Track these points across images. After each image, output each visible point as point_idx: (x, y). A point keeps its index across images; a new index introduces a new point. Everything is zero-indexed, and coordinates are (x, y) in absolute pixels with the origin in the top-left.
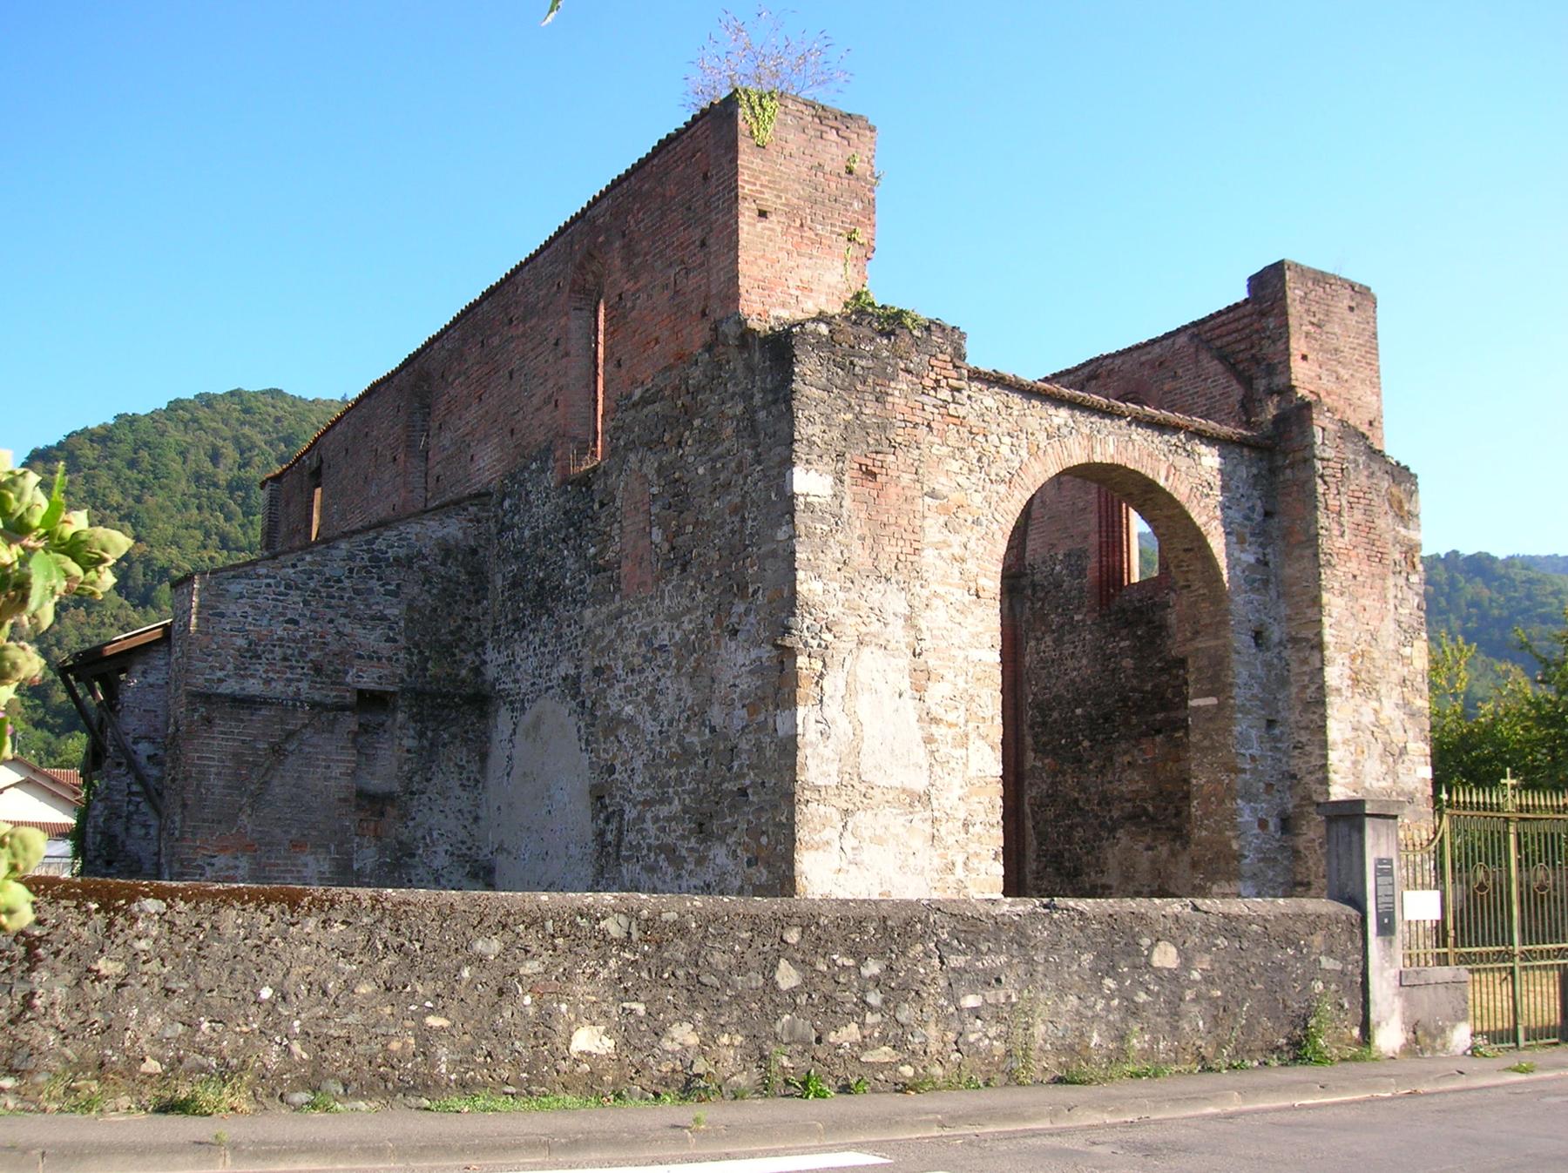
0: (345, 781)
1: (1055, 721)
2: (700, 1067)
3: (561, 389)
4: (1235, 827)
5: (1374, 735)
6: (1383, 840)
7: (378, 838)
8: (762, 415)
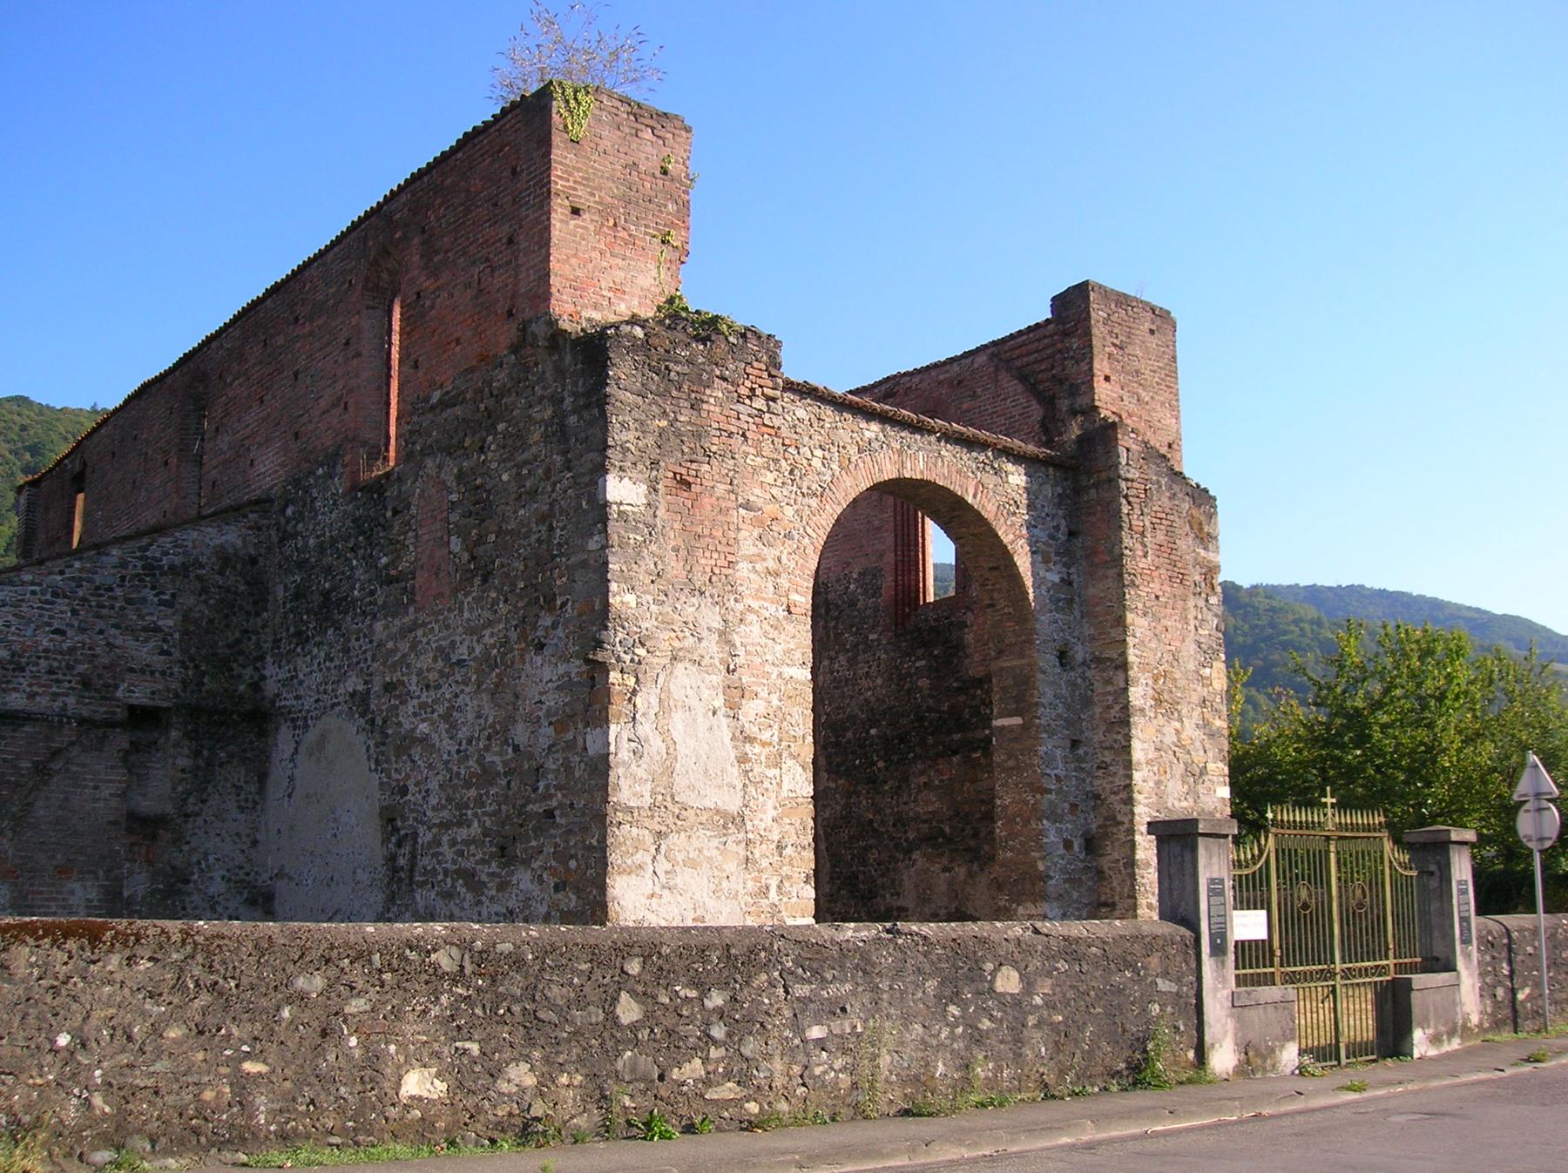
0: (114, 803)
1: (849, 742)
2: (538, 1109)
3: (351, 390)
4: (1040, 847)
5: (1176, 759)
6: (1215, 860)
7: (150, 863)
8: (573, 419)
